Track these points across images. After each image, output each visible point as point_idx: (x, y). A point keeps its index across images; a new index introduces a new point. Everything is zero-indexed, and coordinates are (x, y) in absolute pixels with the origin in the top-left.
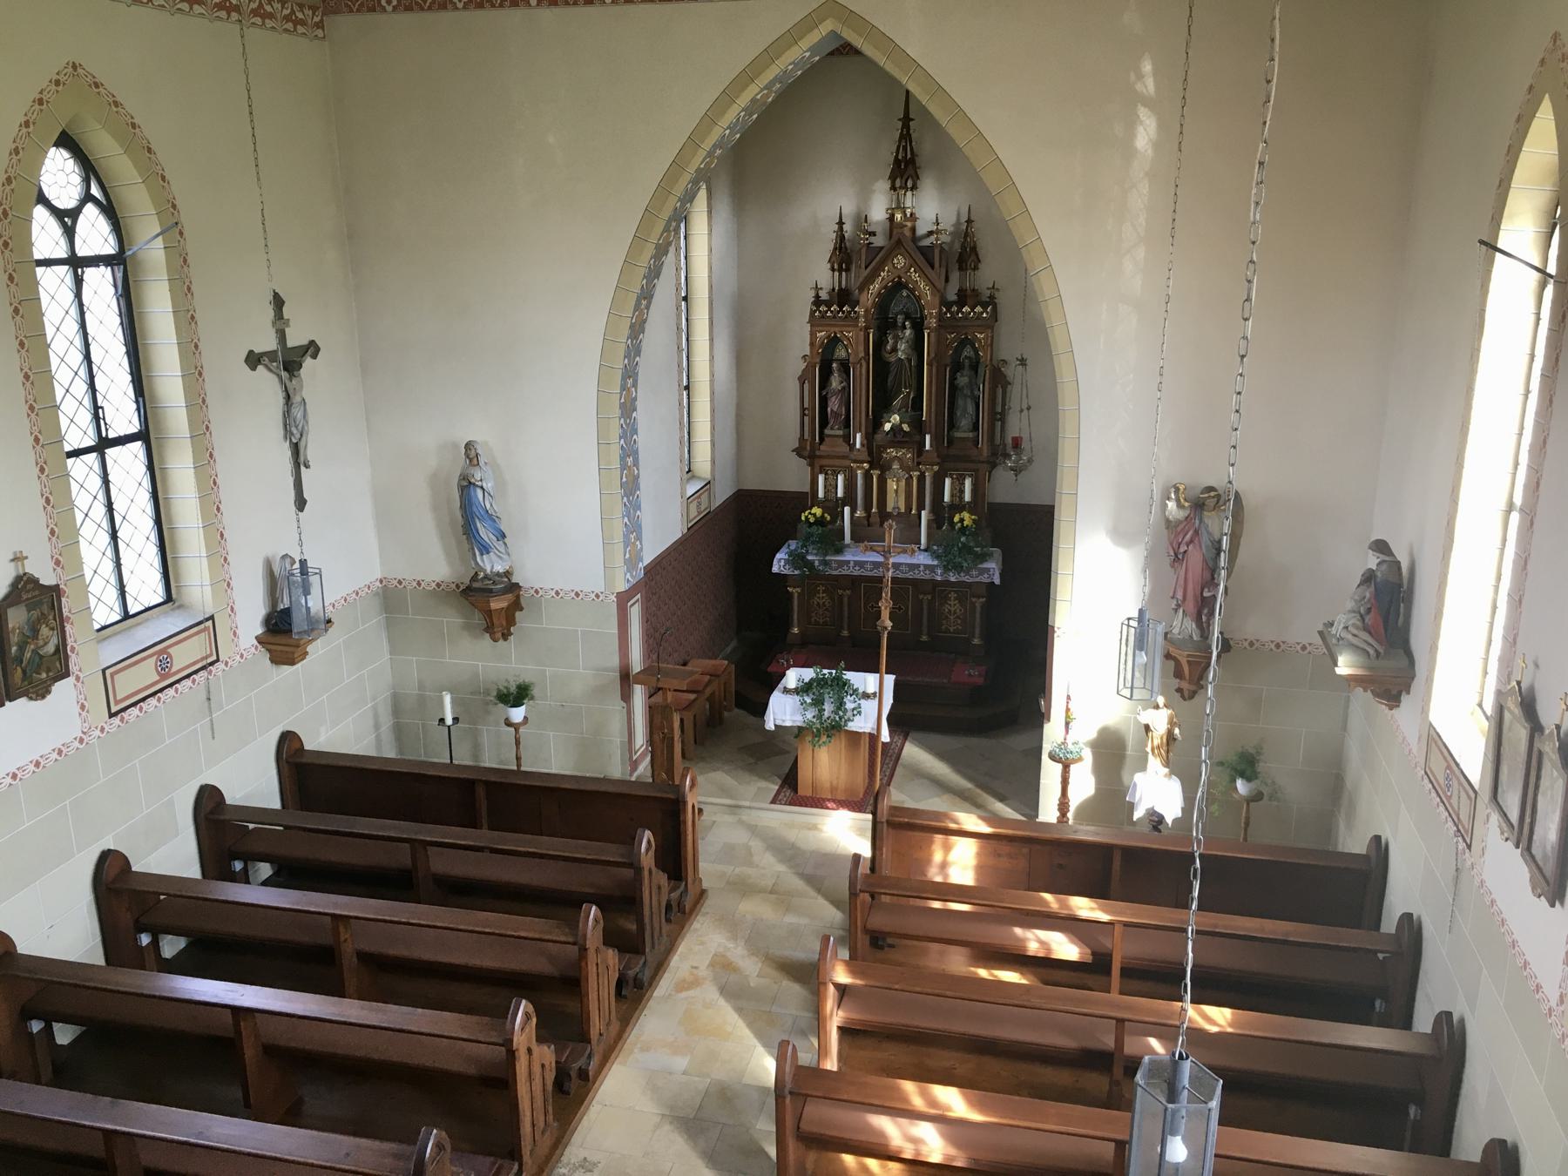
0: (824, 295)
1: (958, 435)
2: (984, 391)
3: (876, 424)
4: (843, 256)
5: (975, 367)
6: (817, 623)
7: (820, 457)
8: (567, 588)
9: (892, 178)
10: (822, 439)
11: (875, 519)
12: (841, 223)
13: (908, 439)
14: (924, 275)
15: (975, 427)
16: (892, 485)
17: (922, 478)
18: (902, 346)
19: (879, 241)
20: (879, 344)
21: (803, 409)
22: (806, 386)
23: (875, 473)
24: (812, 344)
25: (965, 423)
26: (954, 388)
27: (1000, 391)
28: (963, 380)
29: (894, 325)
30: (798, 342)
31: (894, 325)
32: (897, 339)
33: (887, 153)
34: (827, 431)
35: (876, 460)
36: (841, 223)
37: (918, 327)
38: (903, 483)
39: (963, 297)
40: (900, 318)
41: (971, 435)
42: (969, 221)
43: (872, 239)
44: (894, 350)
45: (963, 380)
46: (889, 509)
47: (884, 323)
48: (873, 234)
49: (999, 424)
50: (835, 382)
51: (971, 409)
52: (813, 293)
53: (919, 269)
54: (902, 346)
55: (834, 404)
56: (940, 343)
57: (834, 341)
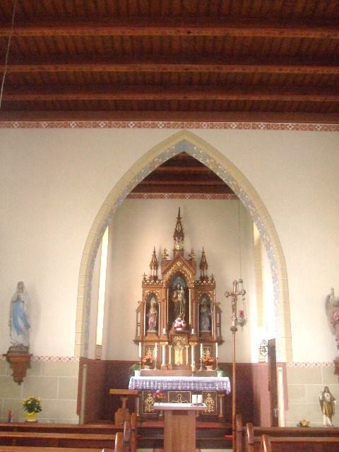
0: (147, 278)
1: (203, 331)
2: (213, 313)
3: (170, 327)
4: (155, 265)
5: (209, 306)
6: (147, 412)
7: (146, 341)
8: (55, 356)
9: (174, 236)
10: (146, 334)
11: (170, 367)
12: (155, 252)
13: (186, 332)
14: (188, 268)
15: (210, 329)
16: (177, 352)
17: (190, 349)
18: (180, 296)
19: (168, 258)
20: (170, 296)
21: (220, 327)
22: (139, 314)
23: (170, 347)
24: (143, 295)
25: (205, 327)
26: (200, 314)
27: (218, 315)
28: (204, 310)
29: (176, 289)
30: (138, 295)
31: (176, 289)
32: (177, 294)
33: (172, 229)
34: (149, 331)
35: (171, 342)
36: (155, 252)
37: (186, 290)
38: (181, 352)
39: (203, 278)
40: (178, 286)
41: (208, 331)
42: (203, 252)
43: (167, 257)
44: (177, 297)
45: (204, 310)
46: (176, 363)
47: (171, 288)
48: (168, 255)
49: (139, 322)
50: (152, 311)
51: (208, 320)
52: (143, 277)
53: (186, 266)
54: (180, 296)
55: (151, 320)
56: (196, 294)
57: (152, 295)
